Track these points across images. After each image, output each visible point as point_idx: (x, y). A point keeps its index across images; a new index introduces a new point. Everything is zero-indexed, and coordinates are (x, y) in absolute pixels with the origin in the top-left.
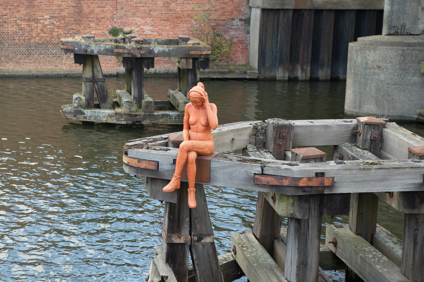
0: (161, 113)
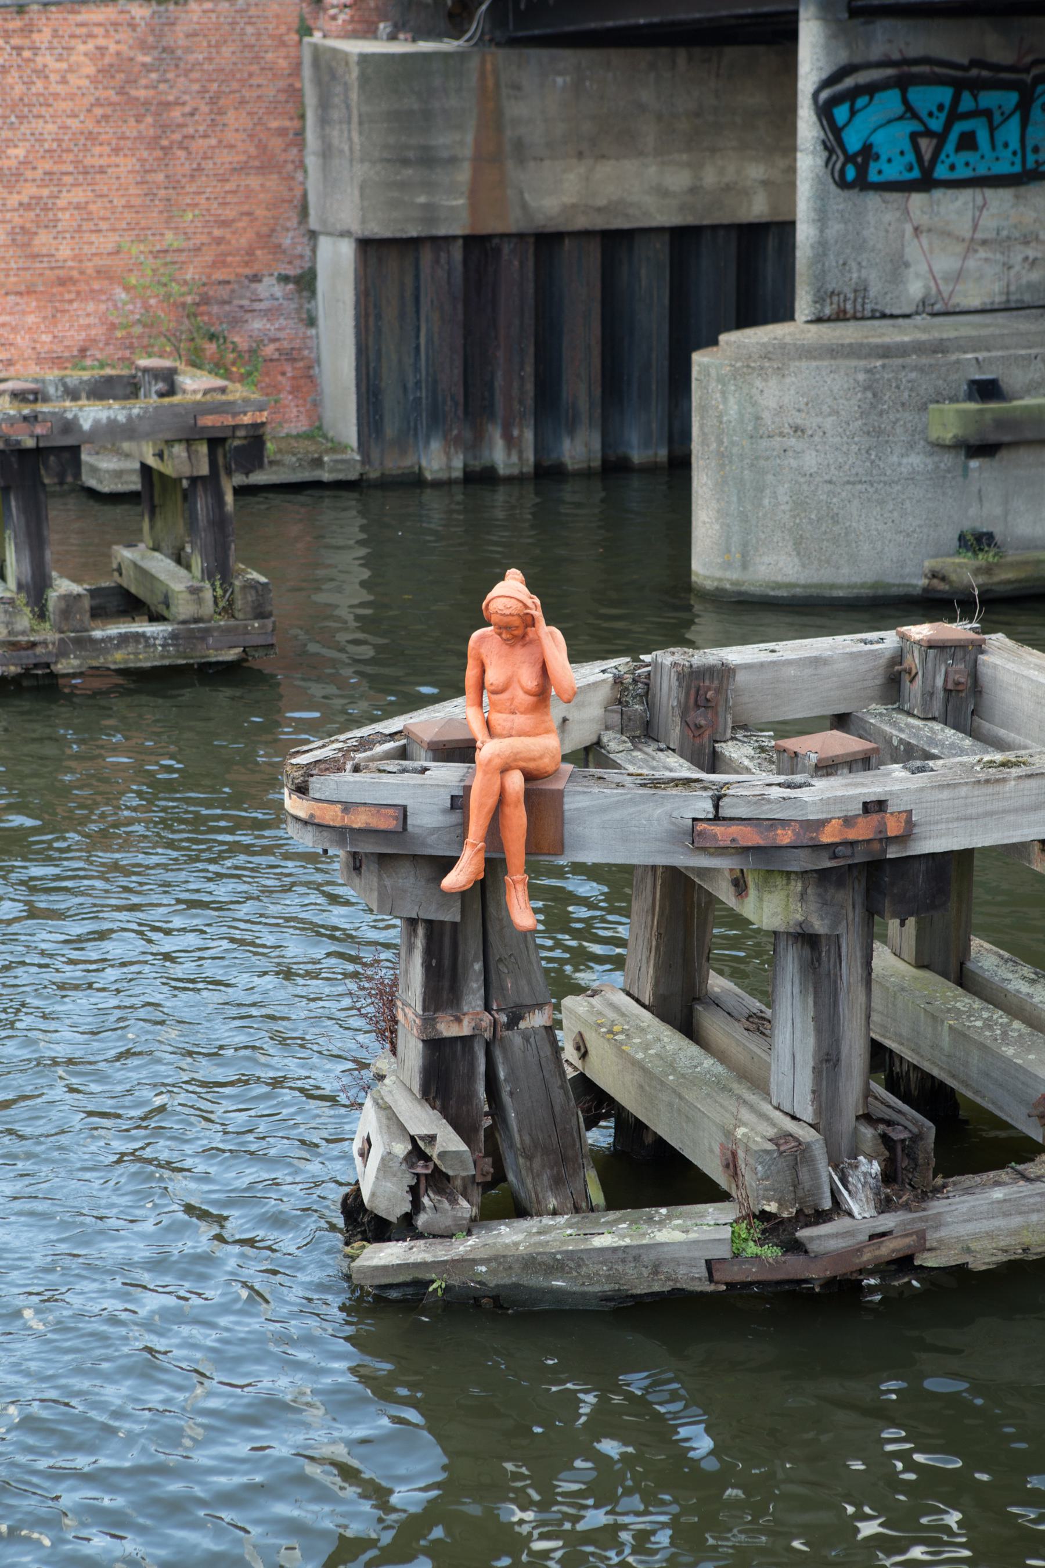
0: (115, 630)
